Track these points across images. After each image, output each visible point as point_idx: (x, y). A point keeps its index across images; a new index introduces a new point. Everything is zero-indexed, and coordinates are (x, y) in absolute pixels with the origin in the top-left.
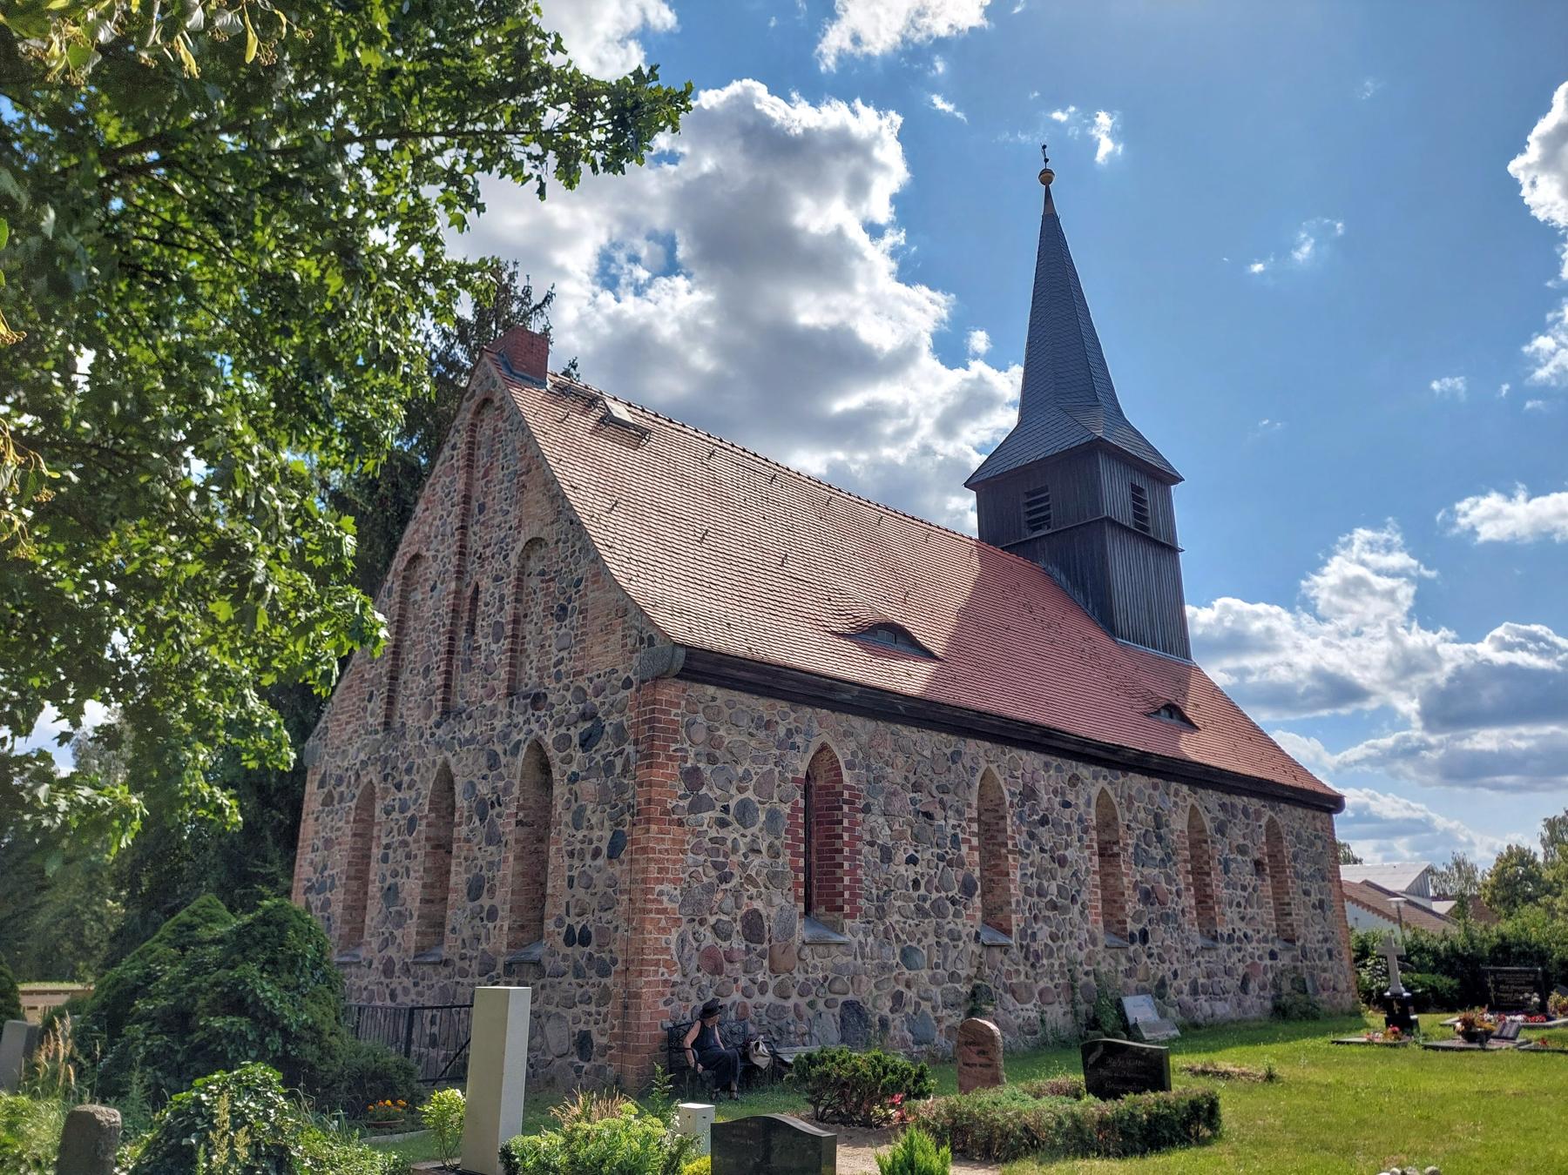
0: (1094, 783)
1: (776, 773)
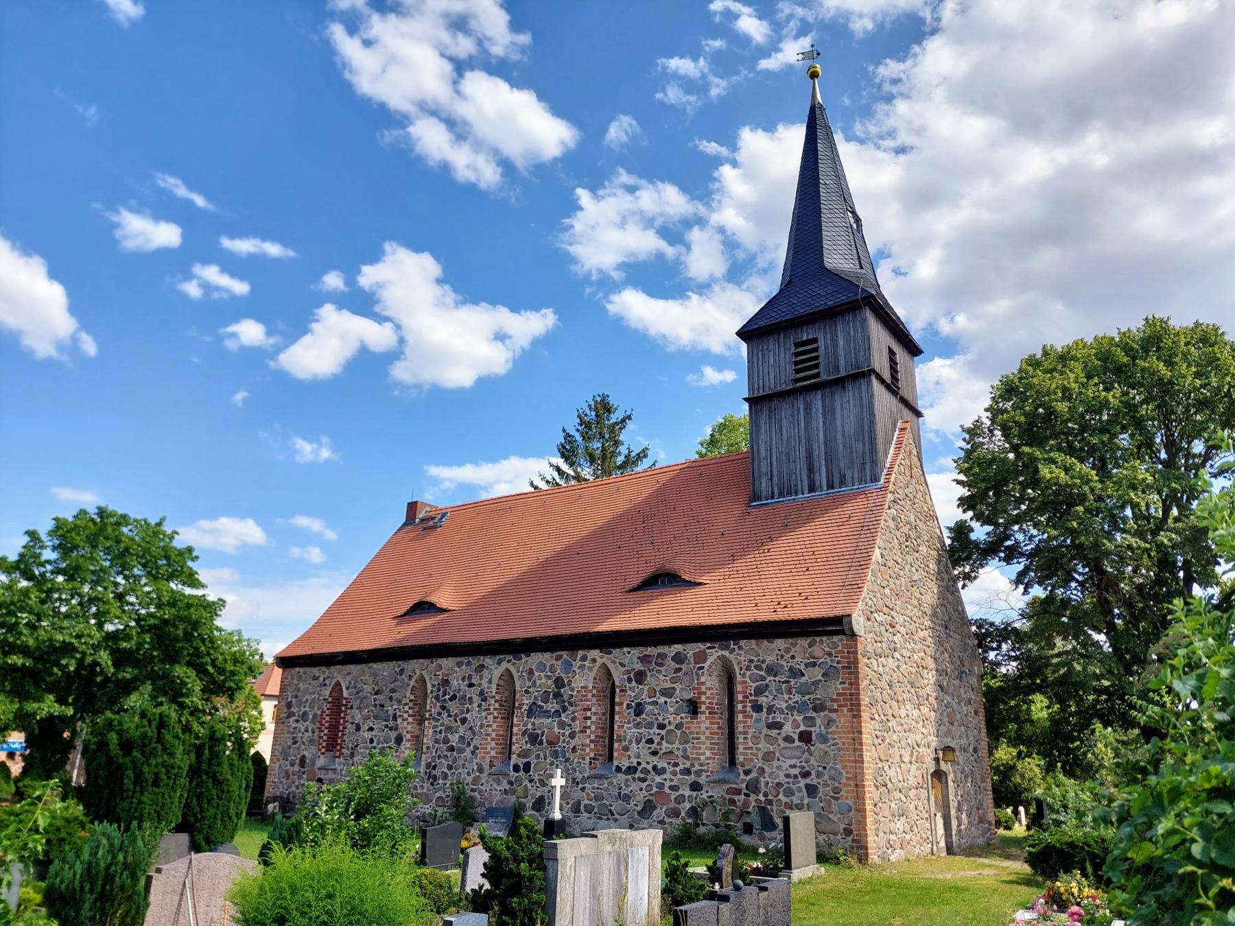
0: (495, 668)
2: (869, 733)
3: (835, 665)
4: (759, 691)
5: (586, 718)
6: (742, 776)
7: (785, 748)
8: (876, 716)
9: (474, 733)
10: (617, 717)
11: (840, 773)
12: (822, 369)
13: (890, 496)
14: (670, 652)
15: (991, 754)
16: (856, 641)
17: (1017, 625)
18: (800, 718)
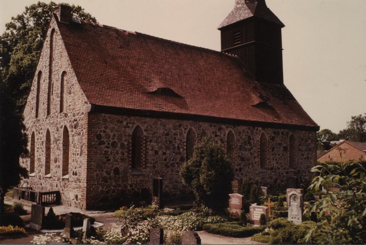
1: (123, 134)
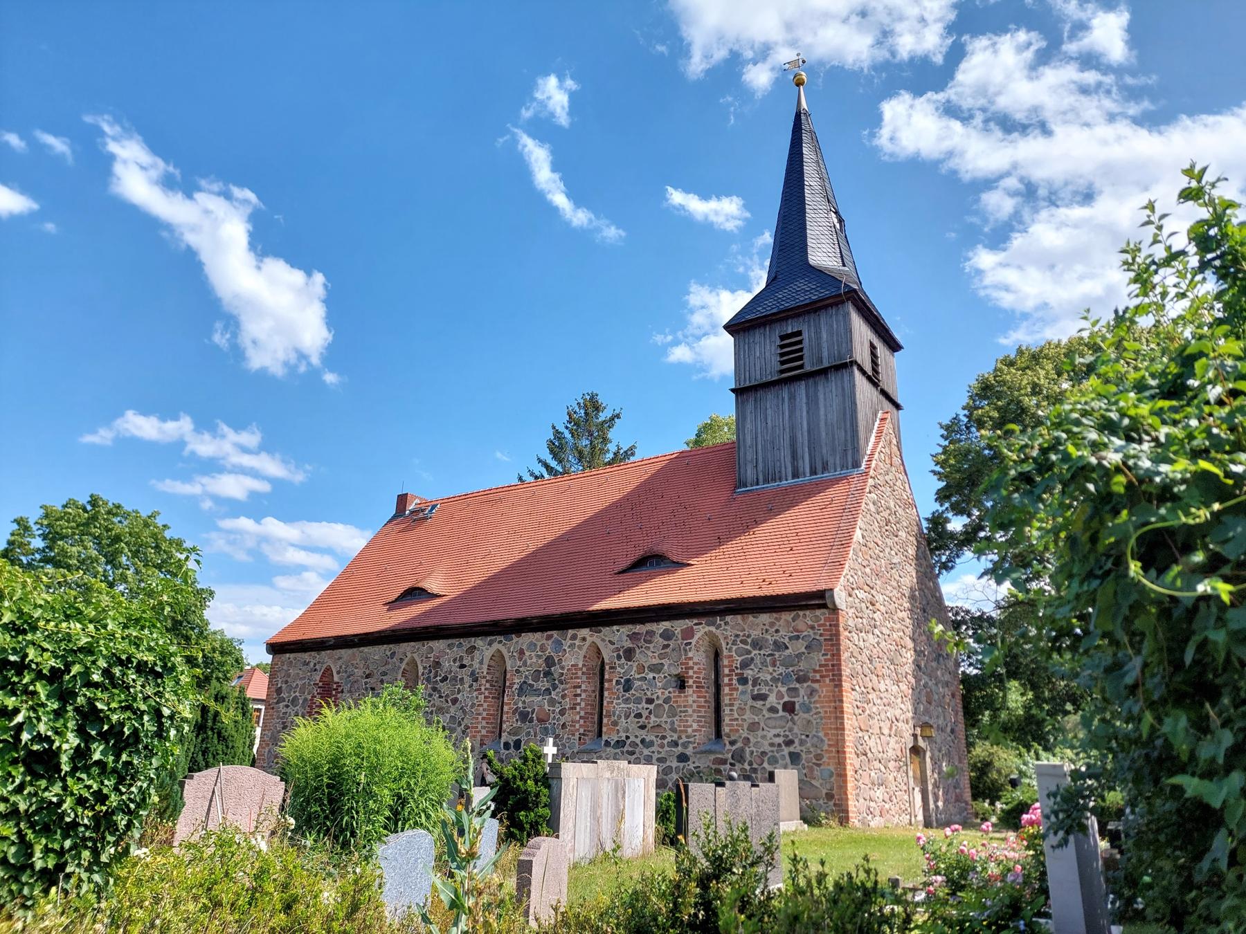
0: (486, 649)
2: (850, 703)
3: (818, 637)
4: (745, 665)
5: (576, 695)
6: (728, 747)
7: (769, 718)
8: (857, 687)
9: (464, 712)
10: (606, 694)
11: (822, 741)
12: (806, 361)
13: (871, 481)
14: (658, 629)
15: (969, 752)
16: (838, 614)
17: (994, 615)
18: (783, 690)
